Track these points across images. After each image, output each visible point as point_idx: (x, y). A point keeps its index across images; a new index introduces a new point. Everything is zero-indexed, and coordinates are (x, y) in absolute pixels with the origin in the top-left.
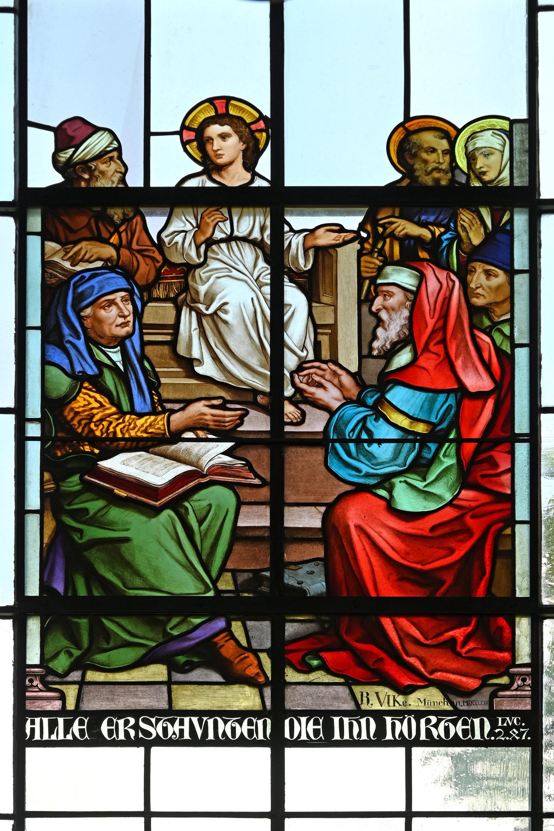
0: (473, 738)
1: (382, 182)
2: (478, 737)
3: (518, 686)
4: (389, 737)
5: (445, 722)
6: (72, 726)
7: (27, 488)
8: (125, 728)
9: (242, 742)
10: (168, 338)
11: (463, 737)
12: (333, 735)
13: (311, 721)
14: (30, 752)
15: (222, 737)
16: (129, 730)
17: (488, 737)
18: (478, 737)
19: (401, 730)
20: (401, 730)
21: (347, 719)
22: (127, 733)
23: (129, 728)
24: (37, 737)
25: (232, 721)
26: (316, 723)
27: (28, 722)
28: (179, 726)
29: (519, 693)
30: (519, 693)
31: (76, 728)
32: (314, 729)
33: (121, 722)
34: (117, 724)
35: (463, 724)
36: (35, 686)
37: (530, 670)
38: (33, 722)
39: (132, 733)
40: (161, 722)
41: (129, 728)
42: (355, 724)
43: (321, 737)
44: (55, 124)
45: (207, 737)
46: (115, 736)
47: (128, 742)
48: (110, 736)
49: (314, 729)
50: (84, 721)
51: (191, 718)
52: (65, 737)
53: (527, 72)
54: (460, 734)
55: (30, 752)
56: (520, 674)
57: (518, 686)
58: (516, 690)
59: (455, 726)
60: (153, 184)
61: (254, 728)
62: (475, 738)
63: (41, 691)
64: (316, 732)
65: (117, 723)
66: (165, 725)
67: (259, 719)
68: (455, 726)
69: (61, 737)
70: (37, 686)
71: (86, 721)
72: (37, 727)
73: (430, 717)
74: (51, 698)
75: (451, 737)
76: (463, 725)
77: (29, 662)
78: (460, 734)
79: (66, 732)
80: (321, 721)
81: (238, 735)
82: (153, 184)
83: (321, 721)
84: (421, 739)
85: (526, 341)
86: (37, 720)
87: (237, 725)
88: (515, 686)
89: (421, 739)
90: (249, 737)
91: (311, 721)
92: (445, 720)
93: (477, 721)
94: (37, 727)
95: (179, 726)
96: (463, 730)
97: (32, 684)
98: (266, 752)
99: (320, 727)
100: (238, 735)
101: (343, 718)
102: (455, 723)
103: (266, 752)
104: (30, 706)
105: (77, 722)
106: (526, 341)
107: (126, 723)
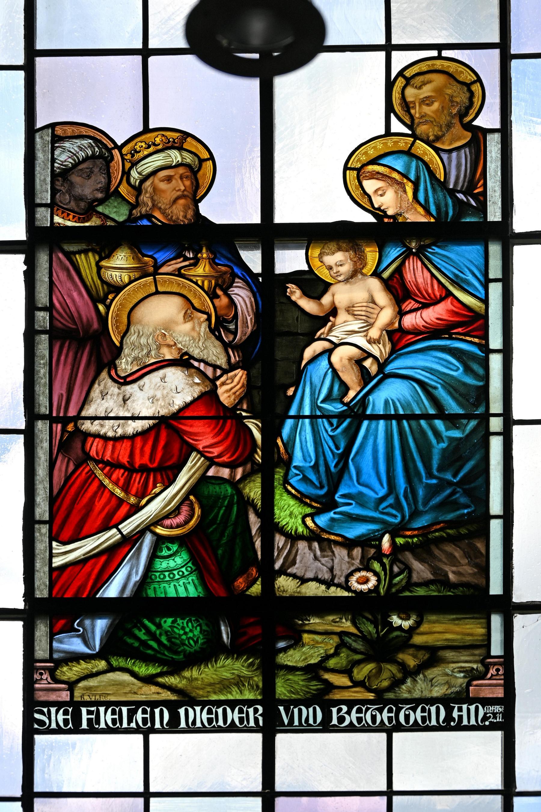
2: (434, 722)
3: (492, 675)
4: (183, 725)
5: (372, 711)
6: (136, 713)
7: (501, 506)
8: (256, 716)
9: (232, 728)
12: (81, 725)
13: (110, 710)
17: (482, 722)
18: (434, 722)
22: (256, 720)
23: (259, 715)
24: (465, 722)
25: (405, 709)
26: (66, 713)
27: (456, 709)
29: (494, 682)
30: (494, 682)
31: (139, 716)
32: (64, 719)
33: (251, 710)
34: (217, 712)
37: (502, 660)
38: (460, 709)
40: (403, 711)
41: (259, 715)
43: (364, 724)
44: (323, 58)
45: (462, 723)
48: (241, 724)
50: (362, 709)
51: (121, 707)
52: (129, 724)
54: (419, 721)
56: (495, 664)
57: (492, 675)
58: (490, 679)
59: (415, 713)
61: (426, 714)
62: (123, 727)
63: (49, 683)
64: (66, 722)
65: (429, 709)
66: (374, 713)
67: (432, 706)
68: (415, 713)
70: (47, 679)
71: (70, 710)
72: (464, 713)
73: (342, 706)
74: (39, 689)
78: (419, 721)
79: (130, 721)
81: (412, 721)
85: (500, 276)
86: (465, 707)
87: (412, 713)
88: (489, 676)
91: (61, 711)
92: (405, 709)
93: (433, 709)
94: (464, 713)
98: (258, 737)
99: (69, 717)
102: (381, 711)
103: (258, 737)
104: (41, 696)
105: (140, 710)
106: (500, 276)
107: (256, 711)
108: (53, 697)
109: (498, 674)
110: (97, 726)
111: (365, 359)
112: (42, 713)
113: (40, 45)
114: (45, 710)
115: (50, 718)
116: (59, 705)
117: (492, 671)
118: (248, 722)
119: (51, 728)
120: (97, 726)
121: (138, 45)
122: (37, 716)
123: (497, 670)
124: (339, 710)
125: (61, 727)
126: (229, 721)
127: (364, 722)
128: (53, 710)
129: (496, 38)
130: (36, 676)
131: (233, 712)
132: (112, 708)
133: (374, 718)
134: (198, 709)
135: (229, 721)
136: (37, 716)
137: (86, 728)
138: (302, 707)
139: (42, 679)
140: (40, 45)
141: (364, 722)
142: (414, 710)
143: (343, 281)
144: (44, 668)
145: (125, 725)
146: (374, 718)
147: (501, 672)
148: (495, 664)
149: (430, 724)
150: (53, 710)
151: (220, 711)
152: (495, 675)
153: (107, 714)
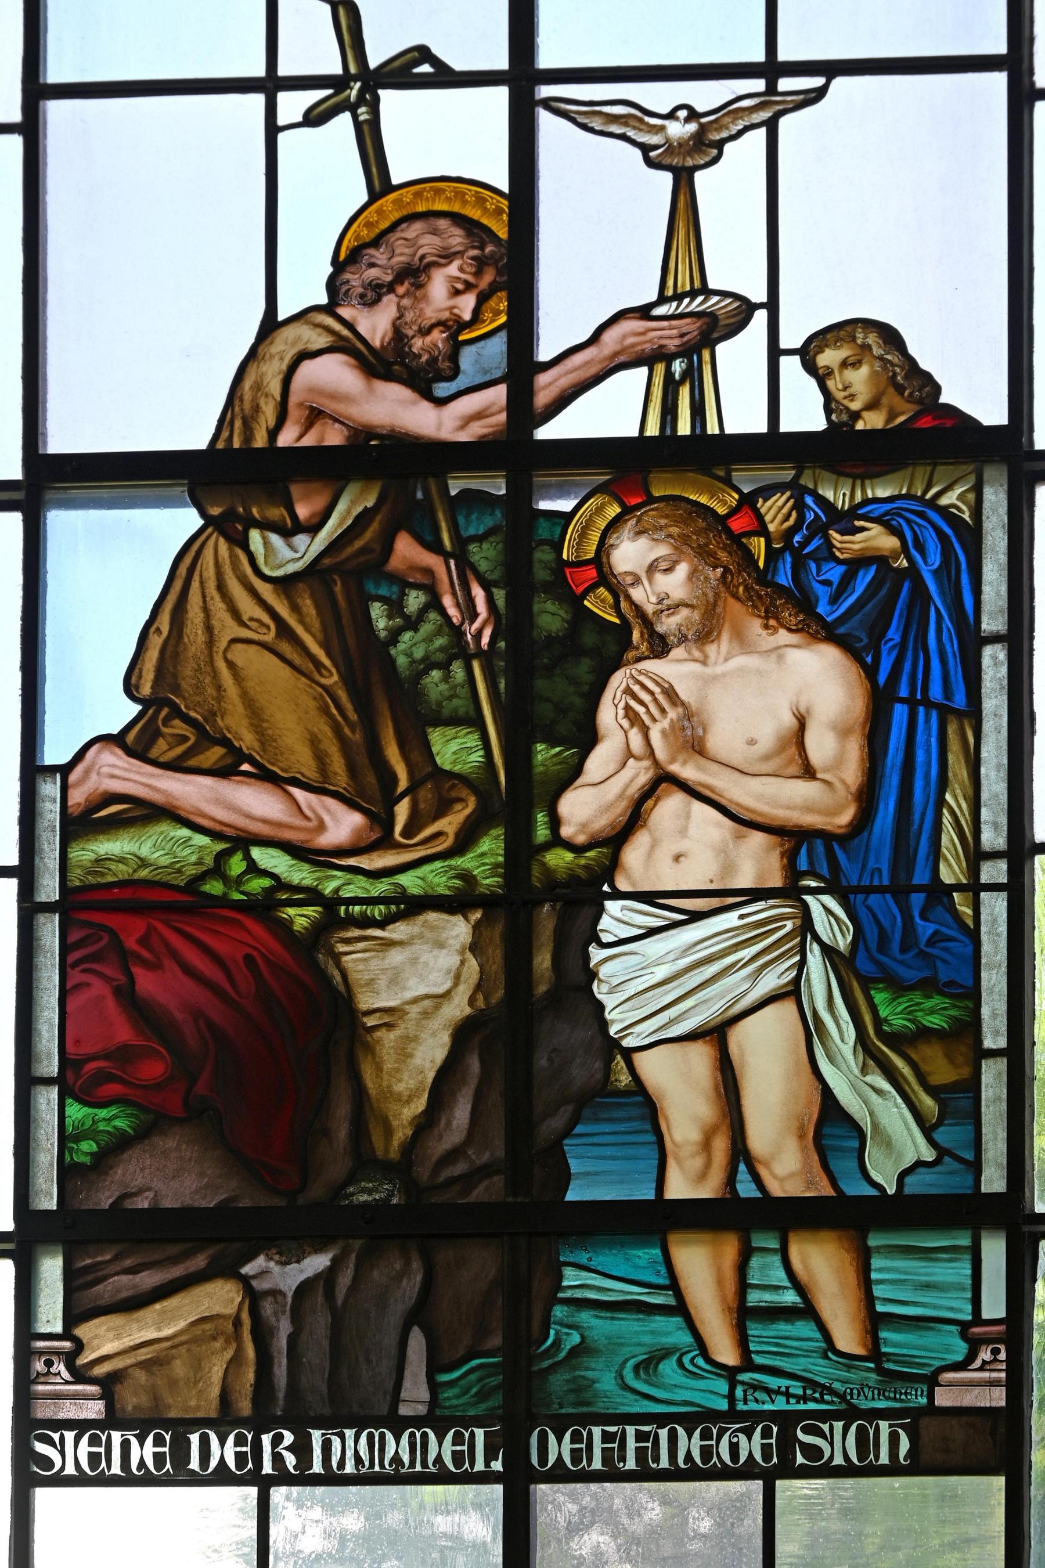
0: (589, 1467)
1: (986, 421)
3: (984, 1362)
10: (934, 715)
11: (859, 1461)
13: (85, 1439)
14: (43, 1497)
15: (685, 1463)
16: (285, 1453)
18: (664, 1463)
19: (142, 1449)
20: (142, 1449)
21: (887, 1423)
22: (277, 1458)
26: (159, 1441)
28: (154, 1446)
30: (986, 1375)
35: (703, 1437)
36: (55, 1375)
39: (290, 1460)
41: (285, 1448)
42: (336, 1442)
46: (104, 1464)
47: (222, 1477)
49: (89, 1453)
52: (487, 1464)
53: (45, 193)
55: (43, 1497)
57: (984, 1362)
58: (981, 1369)
60: (785, 427)
63: (67, 1383)
64: (159, 1458)
66: (735, 1440)
69: (480, 1466)
75: (550, 1465)
76: (90, 1445)
77: (43, 1328)
80: (168, 1438)
81: (743, 1458)
82: (785, 427)
83: (168, 1438)
84: (264, 1472)
87: (742, 1438)
88: (978, 1363)
89: (264, 1472)
90: (155, 1468)
91: (85, 1439)
95: (154, 1446)
96: (237, 1454)
97: (49, 1370)
100: (743, 1458)
101: (345, 1430)
104: (43, 1411)
107: (277, 1440)
108: (69, 1411)
109: (995, 1360)
110: (654, 1466)
111: (455, 721)
112: (50, 1442)
113: (55, 74)
114: (56, 1437)
115: (62, 1453)
116: (80, 1426)
117: (985, 1355)
118: (590, 1460)
119: (66, 1472)
120: (654, 1466)
121: (258, 69)
122: (41, 1448)
123: (996, 1352)
124: (277, 1440)
125: (86, 1473)
126: (214, 1463)
127: (715, 1459)
128: (70, 1436)
129: (999, 46)
130: (39, 1366)
131: (222, 1443)
132: (369, 1430)
133: (734, 1448)
134: (349, 1433)
135: (214, 1463)
136: (41, 1448)
137: (270, 1471)
138: (428, 1430)
139: (49, 1373)
140: (55, 74)
141: (715, 1459)
142: (749, 1433)
143: (288, 562)
144: (58, 1353)
145: (480, 1466)
146: (734, 1448)
147: (1002, 1356)
148: (988, 1341)
149: (589, 1467)
150: (70, 1436)
151: (663, 1433)
152: (989, 1363)
153: (848, 1436)
